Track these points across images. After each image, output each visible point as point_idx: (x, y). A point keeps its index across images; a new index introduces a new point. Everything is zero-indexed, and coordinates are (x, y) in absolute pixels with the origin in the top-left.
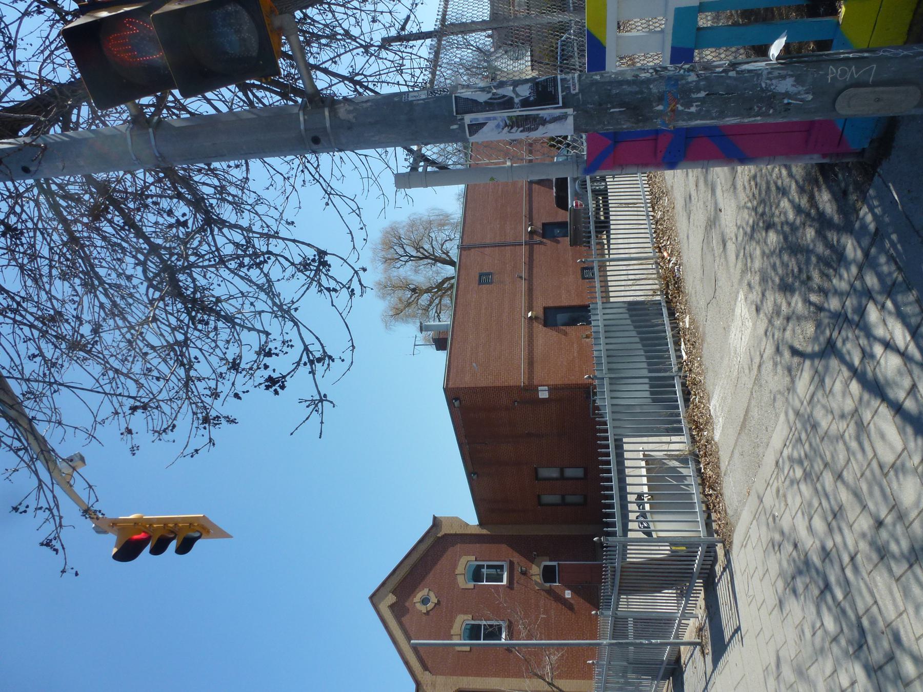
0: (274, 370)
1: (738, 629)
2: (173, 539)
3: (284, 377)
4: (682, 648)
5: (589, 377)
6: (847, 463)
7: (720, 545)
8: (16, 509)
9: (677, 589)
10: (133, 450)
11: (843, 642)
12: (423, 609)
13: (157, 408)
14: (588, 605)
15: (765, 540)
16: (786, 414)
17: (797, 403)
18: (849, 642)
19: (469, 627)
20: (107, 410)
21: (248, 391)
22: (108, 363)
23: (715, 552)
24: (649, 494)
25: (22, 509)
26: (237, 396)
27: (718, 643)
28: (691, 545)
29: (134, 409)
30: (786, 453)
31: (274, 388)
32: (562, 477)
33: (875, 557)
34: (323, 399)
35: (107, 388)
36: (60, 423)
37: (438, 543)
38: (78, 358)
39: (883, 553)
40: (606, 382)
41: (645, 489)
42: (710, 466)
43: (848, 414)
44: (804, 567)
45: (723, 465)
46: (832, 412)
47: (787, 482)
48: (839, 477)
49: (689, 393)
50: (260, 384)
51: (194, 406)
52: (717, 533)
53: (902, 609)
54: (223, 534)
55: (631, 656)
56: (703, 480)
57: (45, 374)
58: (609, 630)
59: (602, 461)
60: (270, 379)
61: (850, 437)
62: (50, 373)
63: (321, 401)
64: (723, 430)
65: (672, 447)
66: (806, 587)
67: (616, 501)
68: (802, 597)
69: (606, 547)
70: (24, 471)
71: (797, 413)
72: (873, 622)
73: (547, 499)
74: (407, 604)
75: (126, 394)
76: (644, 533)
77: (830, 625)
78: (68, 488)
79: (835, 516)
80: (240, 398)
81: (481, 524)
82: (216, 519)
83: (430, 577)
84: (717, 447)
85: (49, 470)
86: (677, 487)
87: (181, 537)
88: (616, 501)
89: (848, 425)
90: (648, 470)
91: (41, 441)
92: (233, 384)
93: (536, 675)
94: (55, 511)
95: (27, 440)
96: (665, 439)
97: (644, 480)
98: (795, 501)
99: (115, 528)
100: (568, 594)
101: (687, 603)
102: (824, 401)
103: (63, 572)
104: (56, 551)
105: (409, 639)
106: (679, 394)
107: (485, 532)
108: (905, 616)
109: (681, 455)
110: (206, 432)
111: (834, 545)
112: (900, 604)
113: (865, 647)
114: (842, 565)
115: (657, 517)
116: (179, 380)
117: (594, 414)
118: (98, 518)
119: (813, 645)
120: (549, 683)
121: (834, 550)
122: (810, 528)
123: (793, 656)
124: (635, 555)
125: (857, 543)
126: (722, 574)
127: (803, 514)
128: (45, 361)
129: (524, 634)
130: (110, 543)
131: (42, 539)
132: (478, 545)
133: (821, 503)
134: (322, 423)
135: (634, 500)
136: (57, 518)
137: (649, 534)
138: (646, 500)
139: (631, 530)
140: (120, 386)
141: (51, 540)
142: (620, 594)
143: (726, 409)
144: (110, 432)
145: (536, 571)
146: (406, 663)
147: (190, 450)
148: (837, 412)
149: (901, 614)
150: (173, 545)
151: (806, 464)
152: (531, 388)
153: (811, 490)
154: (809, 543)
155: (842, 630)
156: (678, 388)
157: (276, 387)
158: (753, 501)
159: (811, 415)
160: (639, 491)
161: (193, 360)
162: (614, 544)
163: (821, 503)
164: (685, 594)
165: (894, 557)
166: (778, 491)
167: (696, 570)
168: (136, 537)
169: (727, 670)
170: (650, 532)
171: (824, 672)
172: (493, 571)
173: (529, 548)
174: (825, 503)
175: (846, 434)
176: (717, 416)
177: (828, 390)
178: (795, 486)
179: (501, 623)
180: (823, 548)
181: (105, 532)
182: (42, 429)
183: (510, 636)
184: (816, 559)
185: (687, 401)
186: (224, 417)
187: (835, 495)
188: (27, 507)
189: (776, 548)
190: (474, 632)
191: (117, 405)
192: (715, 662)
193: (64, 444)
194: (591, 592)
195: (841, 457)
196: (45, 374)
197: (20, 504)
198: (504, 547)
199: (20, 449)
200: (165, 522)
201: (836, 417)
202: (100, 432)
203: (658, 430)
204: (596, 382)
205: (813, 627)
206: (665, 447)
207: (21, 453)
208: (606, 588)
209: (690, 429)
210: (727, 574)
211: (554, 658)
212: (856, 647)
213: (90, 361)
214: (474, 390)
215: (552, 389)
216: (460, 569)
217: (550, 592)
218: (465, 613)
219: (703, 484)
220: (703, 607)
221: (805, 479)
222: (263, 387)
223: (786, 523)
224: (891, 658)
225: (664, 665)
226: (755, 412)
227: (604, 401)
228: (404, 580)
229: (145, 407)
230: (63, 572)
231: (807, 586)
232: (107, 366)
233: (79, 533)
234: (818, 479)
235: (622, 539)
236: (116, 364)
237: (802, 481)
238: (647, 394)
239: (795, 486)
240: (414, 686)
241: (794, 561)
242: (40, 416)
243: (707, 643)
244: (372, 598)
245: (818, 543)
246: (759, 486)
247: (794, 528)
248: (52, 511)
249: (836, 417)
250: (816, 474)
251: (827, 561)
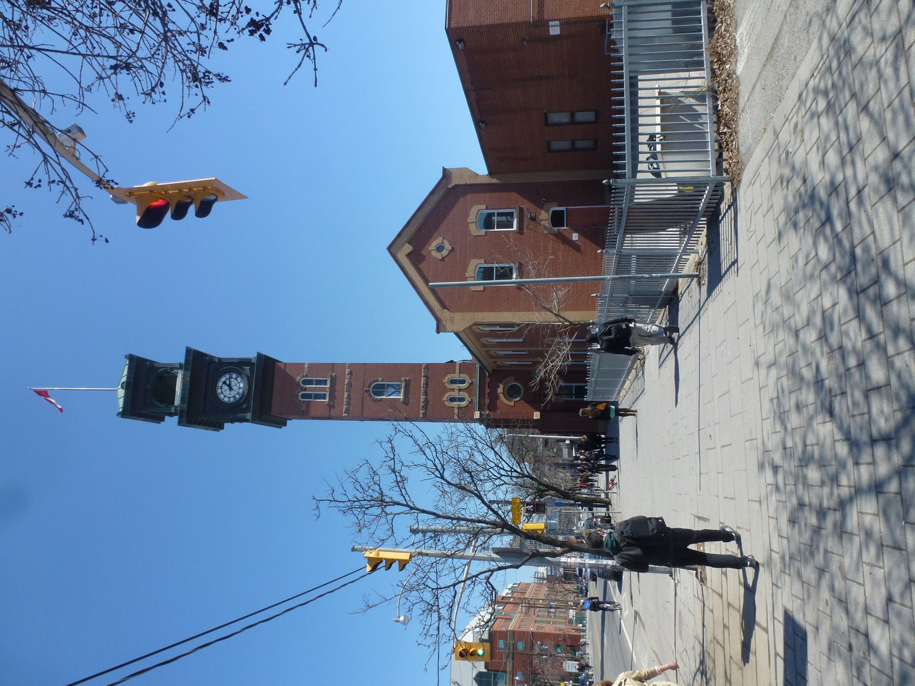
0: (257, 14)
1: (736, 261)
2: (190, 203)
3: (268, 19)
4: (680, 280)
5: (606, 6)
6: (877, 93)
7: (728, 184)
8: (29, 184)
9: (681, 227)
10: (130, 116)
11: (833, 268)
12: (439, 256)
13: (142, 67)
14: (594, 246)
15: (774, 177)
16: (820, 39)
17: (835, 25)
18: (839, 268)
19: (482, 270)
20: (89, 76)
21: (232, 40)
22: (75, 19)
23: (723, 191)
24: (662, 135)
25: (35, 183)
26: (221, 46)
27: (714, 273)
28: (699, 185)
29: (115, 68)
30: (811, 84)
31: (259, 33)
32: (573, 122)
33: (883, 189)
34: (313, 42)
35: (82, 49)
36: (44, 91)
37: (449, 193)
38: (43, 18)
39: (890, 183)
40: (624, 11)
41: (658, 129)
42: (727, 103)
43: (890, 37)
44: (810, 199)
45: (742, 102)
46: (872, 35)
47: (808, 116)
48: (865, 109)
49: (715, 21)
50: (243, 29)
51: (180, 64)
52: (727, 170)
53: (897, 237)
54: (237, 196)
55: (632, 289)
56: (719, 118)
57: (11, 38)
58: (613, 267)
59: (615, 109)
60: (253, 23)
61: (886, 63)
62: (17, 36)
63: (311, 44)
64: (747, 62)
65: (691, 83)
66: (808, 221)
67: (627, 133)
68: (802, 230)
69: (615, 189)
70: (27, 147)
71: (833, 39)
72: (866, 250)
73: (557, 145)
74: (423, 252)
75: (105, 54)
76: (653, 174)
77: (824, 252)
78: (75, 160)
79: (851, 149)
80: (225, 48)
81: (491, 173)
82: (228, 181)
83: (443, 226)
84: (738, 82)
85: (49, 142)
86: (691, 126)
87: (199, 200)
88: (627, 133)
89: (887, 49)
90: (663, 109)
91: (33, 114)
92: (215, 32)
93: (544, 308)
94: (68, 183)
95: (17, 113)
96: (686, 75)
97: (658, 120)
98: (812, 135)
99: (133, 197)
100: (575, 237)
101: (689, 240)
102: (865, 21)
103: (94, 240)
104: (81, 221)
105: (426, 281)
106: (704, 23)
107: (495, 181)
108: (898, 244)
109: (698, 92)
110: (198, 91)
111: (844, 178)
112: (897, 233)
113: (853, 274)
114: (847, 199)
115: (667, 158)
116: (158, 36)
117: (609, 47)
118: (112, 188)
119: (804, 271)
120: (556, 315)
121: (843, 184)
122: (823, 163)
123: (783, 283)
124: (643, 196)
125: (867, 176)
126: (727, 211)
127: (818, 149)
128: (6, 22)
129: (533, 273)
130: (132, 213)
131: (64, 211)
132: (488, 194)
133: (838, 137)
134: (315, 69)
135: (645, 141)
136: (73, 190)
137: (657, 174)
138: (657, 140)
139: (640, 172)
140: (95, 45)
141: (73, 212)
142: (625, 233)
143: (754, 37)
144: (99, 97)
145: (545, 216)
146: (426, 303)
147: (186, 110)
148: (878, 35)
149: (894, 243)
150: (192, 209)
151: (831, 95)
152: (542, 24)
153: (832, 123)
154: (819, 177)
155: (834, 259)
156: (703, 15)
157: (261, 31)
158: (769, 136)
159: (847, 41)
160: (652, 132)
161: (168, 8)
162: (622, 186)
163: (838, 137)
164: (688, 232)
165: (903, 188)
166: (796, 126)
167: (703, 209)
168: (155, 204)
169: (720, 297)
170: (658, 171)
171: (809, 296)
172: (503, 218)
173: (537, 195)
174: (843, 136)
175: (883, 60)
176: (742, 46)
177: (873, 8)
178: (815, 120)
179: (512, 265)
180: (832, 183)
181: (124, 202)
182: (29, 99)
183: (521, 275)
184: (822, 193)
185: (711, 29)
186: (216, 75)
187: (855, 128)
188: (40, 181)
189: (785, 184)
190: (487, 274)
191: (99, 70)
192: (710, 291)
193: (60, 117)
194: (598, 233)
195: (871, 86)
196: (11, 38)
197: (32, 179)
198: (514, 195)
199: (14, 125)
200: (180, 187)
201: (876, 40)
202: (89, 98)
203: (677, 64)
204: (613, 12)
205: (807, 257)
206: (682, 83)
207: (16, 128)
208: (613, 227)
209: (712, 62)
210: (731, 212)
211: (560, 294)
212: (845, 272)
213: (57, 21)
214: (478, 29)
215: (565, 24)
216: (472, 217)
217: (558, 235)
218: (477, 258)
219: (718, 122)
220: (704, 243)
221: (827, 112)
222: (246, 32)
223: (798, 159)
224: (876, 281)
225: (662, 296)
226: (785, 41)
227: (621, 35)
228: (419, 230)
229: (128, 67)
230: (94, 240)
231: (808, 220)
232: (77, 27)
233: (98, 203)
234: (841, 111)
235: (632, 180)
236: (87, 22)
237: (824, 115)
238: (668, 24)
239: (815, 120)
240: (434, 322)
241: (800, 195)
242: (21, 86)
243: (704, 275)
244: (389, 248)
245: (827, 178)
246: (777, 121)
247: (806, 163)
248: (65, 182)
249: (876, 40)
250: (840, 106)
251: (834, 194)
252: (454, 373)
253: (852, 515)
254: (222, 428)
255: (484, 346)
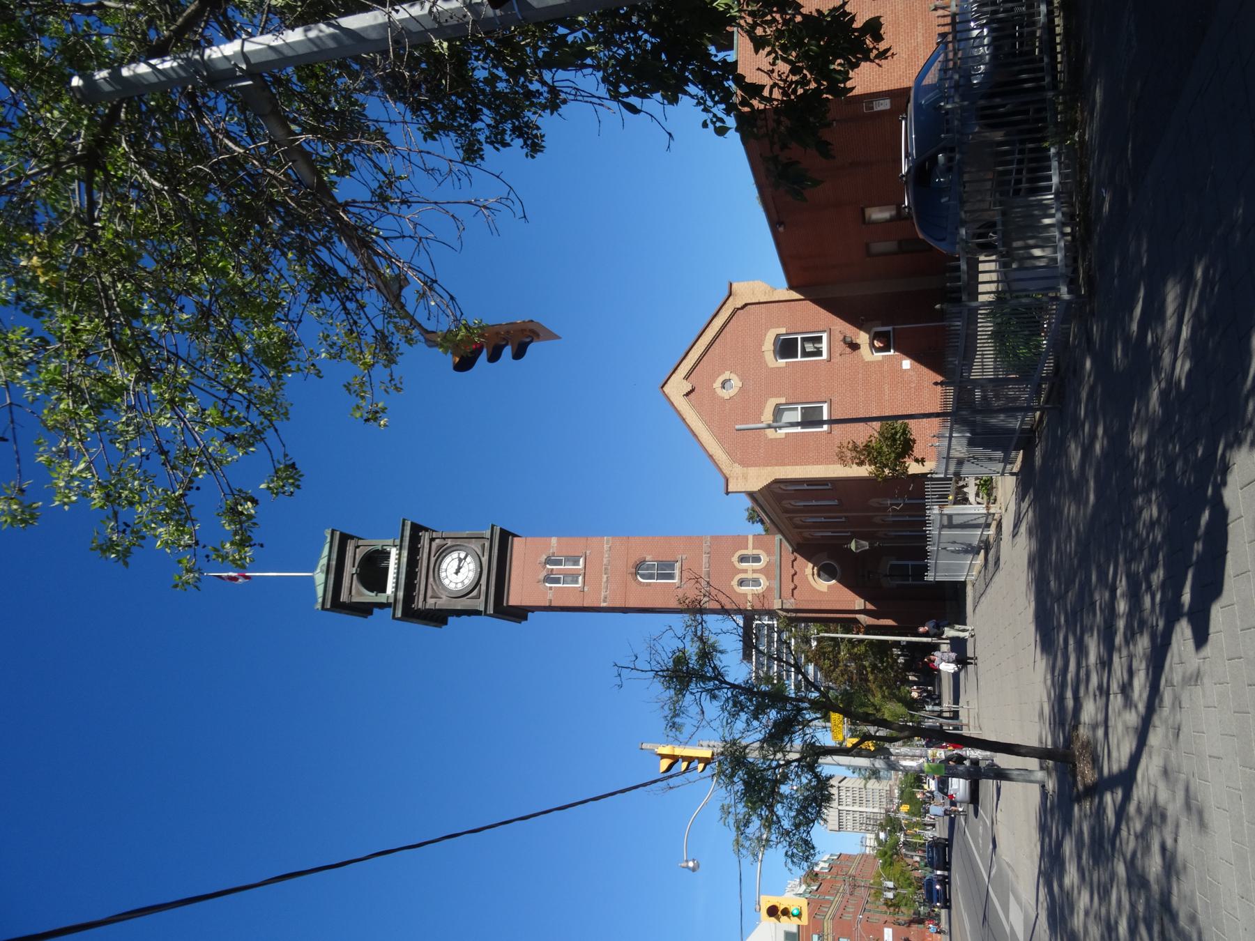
130: (450, 359)
150: (507, 352)
225: (1017, 435)
252: (746, 548)
253: (881, 211)
254: (446, 624)
255: (786, 511)
